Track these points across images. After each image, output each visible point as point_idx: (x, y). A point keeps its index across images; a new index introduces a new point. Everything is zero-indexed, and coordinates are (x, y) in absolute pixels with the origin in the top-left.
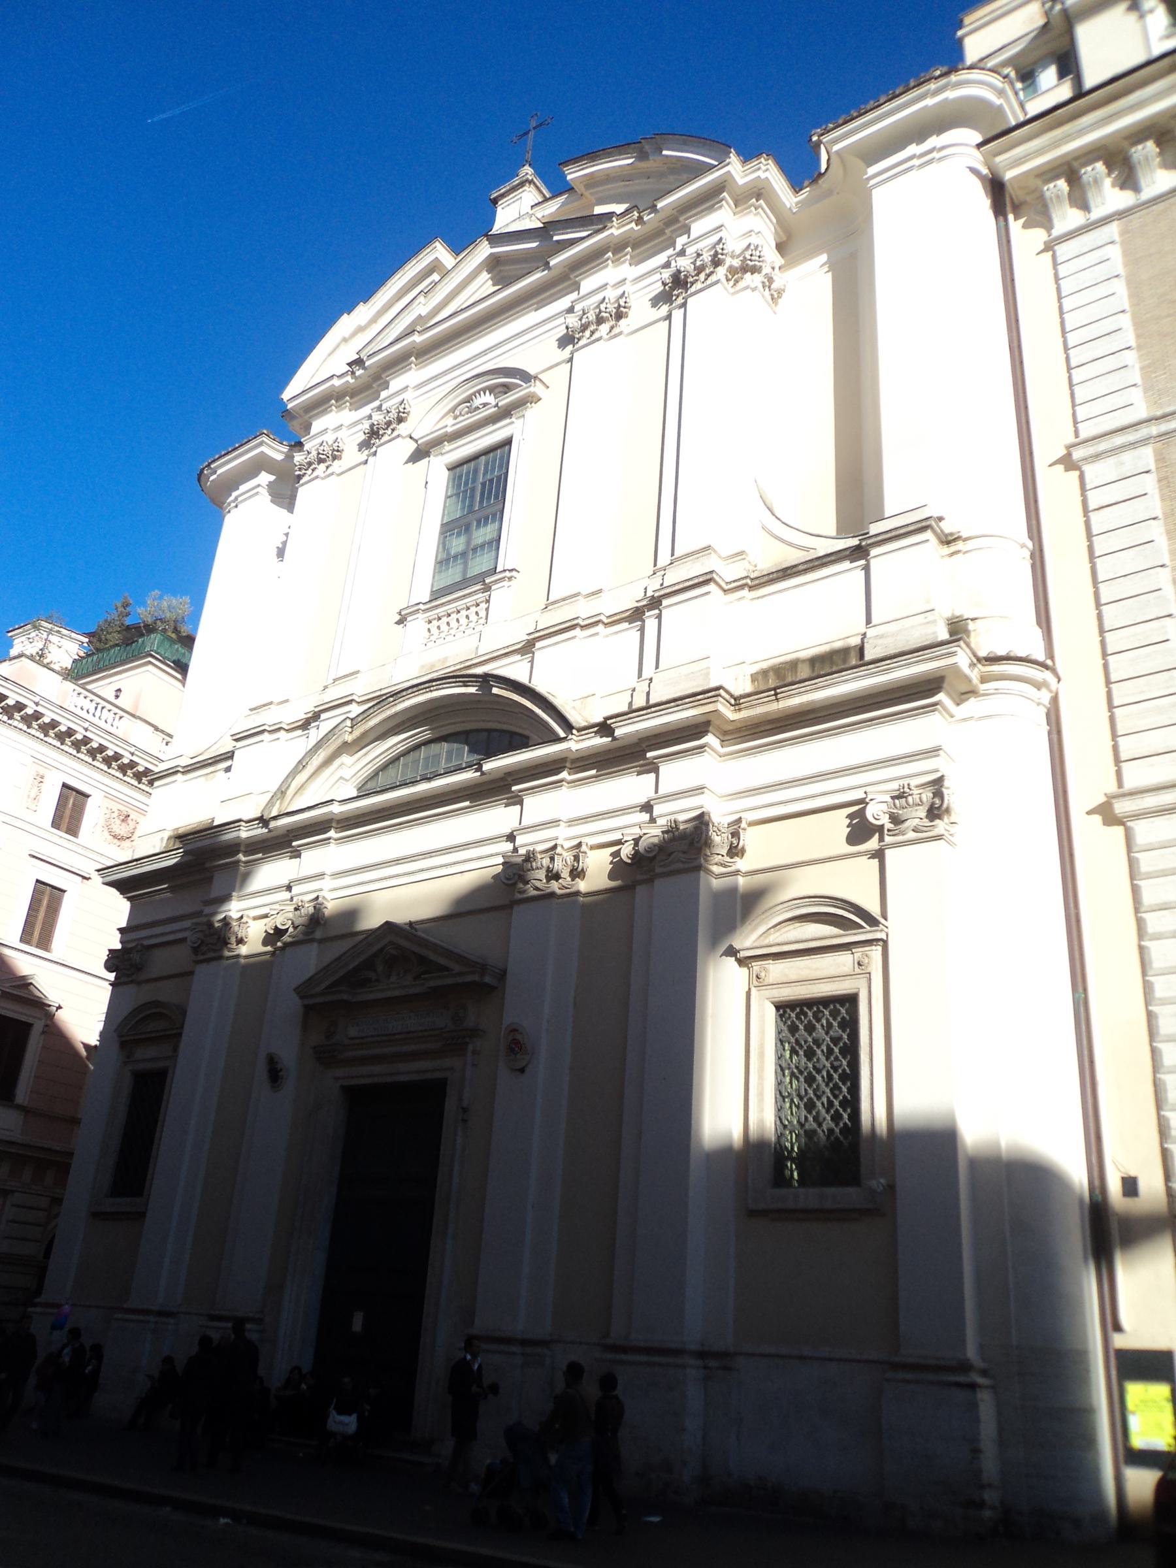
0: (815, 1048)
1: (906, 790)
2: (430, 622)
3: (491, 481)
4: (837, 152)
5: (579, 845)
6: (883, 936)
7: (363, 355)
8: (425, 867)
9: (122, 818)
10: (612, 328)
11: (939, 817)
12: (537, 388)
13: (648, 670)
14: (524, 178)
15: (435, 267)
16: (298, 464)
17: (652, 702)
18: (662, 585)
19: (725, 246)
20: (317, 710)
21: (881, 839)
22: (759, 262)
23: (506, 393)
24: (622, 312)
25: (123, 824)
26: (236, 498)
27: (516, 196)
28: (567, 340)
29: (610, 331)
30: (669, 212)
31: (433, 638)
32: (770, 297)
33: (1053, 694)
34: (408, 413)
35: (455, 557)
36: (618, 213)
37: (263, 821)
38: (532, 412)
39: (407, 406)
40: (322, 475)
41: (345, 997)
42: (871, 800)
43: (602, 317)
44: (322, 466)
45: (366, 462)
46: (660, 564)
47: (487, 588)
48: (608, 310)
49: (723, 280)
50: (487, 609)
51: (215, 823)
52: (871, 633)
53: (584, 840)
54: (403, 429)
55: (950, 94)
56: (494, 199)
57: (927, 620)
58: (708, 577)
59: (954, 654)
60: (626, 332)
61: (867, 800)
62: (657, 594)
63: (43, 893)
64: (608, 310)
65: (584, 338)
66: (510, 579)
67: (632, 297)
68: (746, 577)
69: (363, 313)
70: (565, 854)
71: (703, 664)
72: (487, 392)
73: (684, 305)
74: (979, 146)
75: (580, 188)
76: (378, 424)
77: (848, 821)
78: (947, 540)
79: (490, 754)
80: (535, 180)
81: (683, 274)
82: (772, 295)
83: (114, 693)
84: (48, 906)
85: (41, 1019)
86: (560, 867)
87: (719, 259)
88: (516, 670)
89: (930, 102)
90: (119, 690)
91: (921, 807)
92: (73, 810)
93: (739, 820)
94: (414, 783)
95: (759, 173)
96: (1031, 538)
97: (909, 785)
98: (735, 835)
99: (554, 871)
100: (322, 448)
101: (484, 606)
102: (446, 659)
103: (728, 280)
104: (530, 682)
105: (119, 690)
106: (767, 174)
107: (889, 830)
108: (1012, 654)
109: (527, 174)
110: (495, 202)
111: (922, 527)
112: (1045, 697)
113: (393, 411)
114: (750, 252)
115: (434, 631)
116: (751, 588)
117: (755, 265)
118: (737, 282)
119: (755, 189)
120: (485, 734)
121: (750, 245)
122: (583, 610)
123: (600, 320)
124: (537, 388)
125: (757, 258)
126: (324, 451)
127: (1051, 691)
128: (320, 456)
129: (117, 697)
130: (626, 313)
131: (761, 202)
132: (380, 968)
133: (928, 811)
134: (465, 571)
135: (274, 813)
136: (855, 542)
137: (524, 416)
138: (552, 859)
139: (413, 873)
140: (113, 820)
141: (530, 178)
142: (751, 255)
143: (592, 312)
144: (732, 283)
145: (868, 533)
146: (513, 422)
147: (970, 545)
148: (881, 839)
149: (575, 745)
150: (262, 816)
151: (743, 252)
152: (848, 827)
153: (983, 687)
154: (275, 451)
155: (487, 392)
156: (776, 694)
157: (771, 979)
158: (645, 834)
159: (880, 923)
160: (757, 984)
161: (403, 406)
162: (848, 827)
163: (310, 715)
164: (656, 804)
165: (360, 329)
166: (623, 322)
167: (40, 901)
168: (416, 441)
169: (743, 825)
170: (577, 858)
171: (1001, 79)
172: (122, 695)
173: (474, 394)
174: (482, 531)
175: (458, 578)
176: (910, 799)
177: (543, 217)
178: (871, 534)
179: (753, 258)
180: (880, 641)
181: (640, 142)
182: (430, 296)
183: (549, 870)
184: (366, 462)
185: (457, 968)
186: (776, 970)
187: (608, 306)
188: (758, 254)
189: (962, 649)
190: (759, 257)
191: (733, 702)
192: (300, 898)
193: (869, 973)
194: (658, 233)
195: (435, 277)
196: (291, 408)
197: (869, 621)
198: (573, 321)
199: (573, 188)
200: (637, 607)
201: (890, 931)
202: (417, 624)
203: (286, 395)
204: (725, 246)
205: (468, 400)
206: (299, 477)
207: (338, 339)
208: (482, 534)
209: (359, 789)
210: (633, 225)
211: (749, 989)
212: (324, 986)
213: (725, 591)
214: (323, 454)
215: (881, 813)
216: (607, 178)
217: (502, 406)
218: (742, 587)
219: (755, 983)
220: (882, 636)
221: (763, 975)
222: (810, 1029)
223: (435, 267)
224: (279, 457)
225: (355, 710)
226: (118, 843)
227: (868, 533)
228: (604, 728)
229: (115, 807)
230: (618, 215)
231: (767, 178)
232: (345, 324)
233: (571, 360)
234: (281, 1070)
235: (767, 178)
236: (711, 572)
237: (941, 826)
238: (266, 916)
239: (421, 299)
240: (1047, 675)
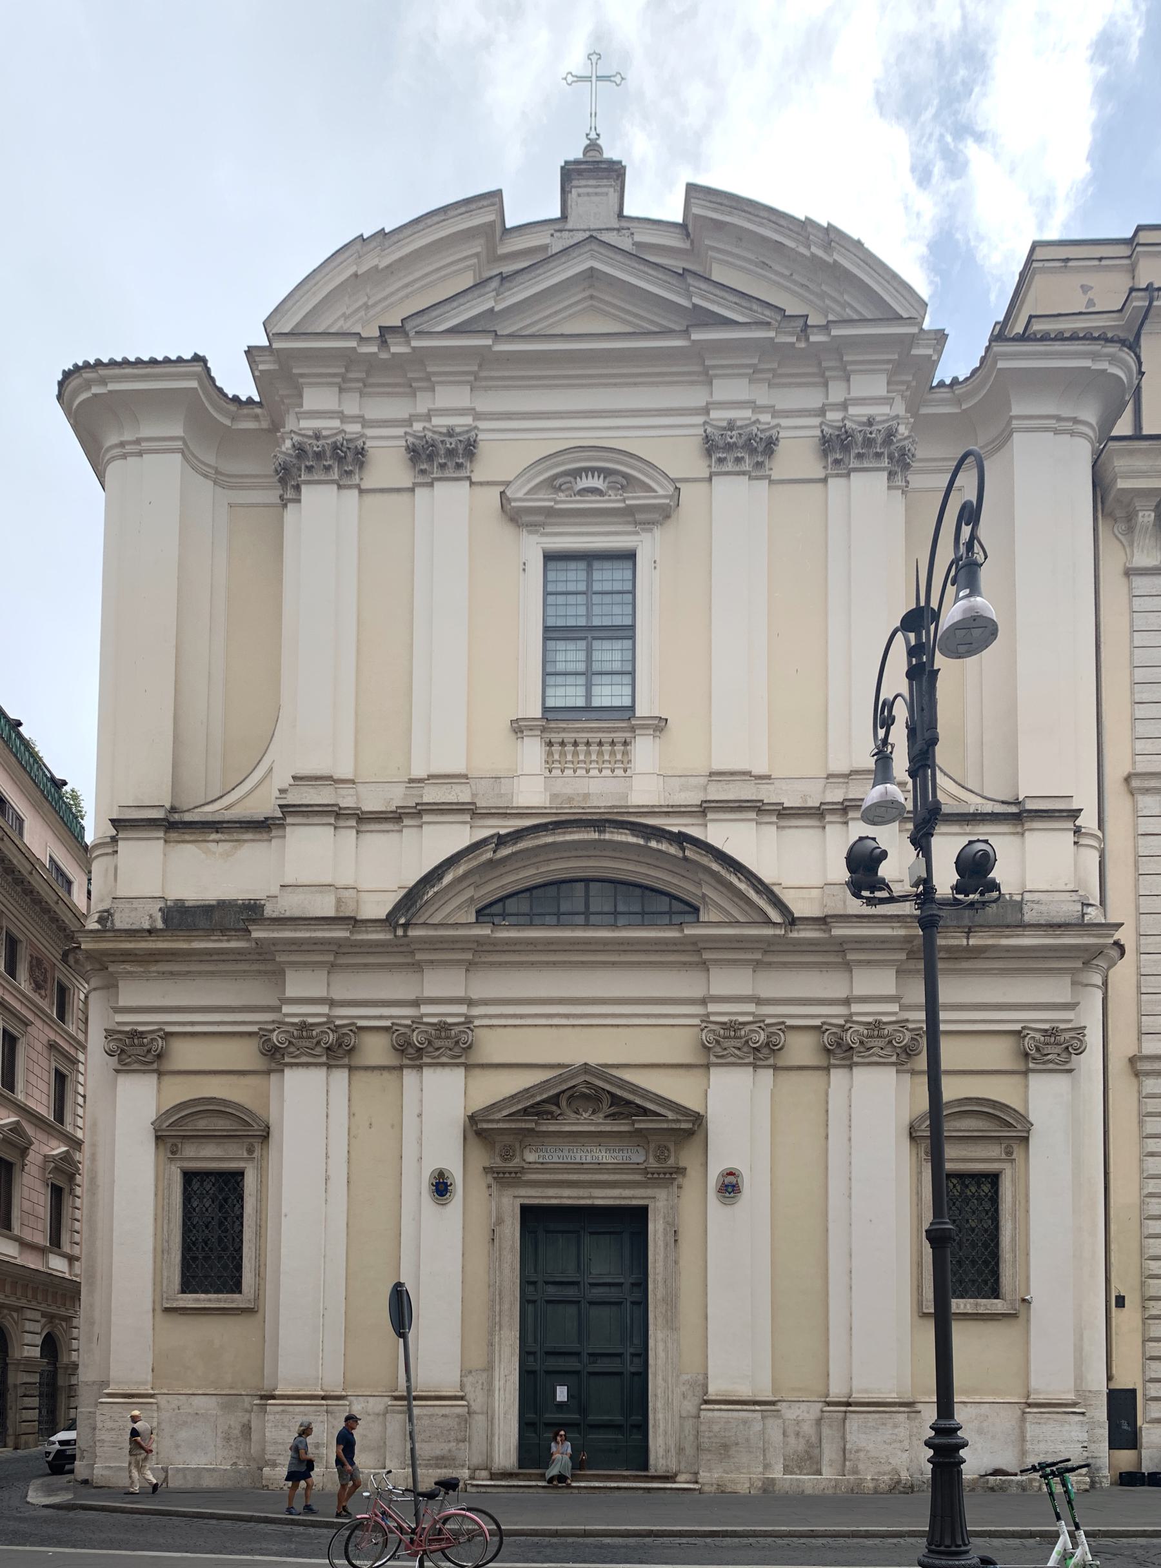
26: (138, 441)
41: (533, 1125)
57: (1073, 899)
72: (590, 474)
132: (564, 1103)
134: (588, 696)
155: (590, 474)
180: (1035, 906)
185: (671, 1115)
186: (189, 1150)
212: (505, 1113)
234: (451, 1184)
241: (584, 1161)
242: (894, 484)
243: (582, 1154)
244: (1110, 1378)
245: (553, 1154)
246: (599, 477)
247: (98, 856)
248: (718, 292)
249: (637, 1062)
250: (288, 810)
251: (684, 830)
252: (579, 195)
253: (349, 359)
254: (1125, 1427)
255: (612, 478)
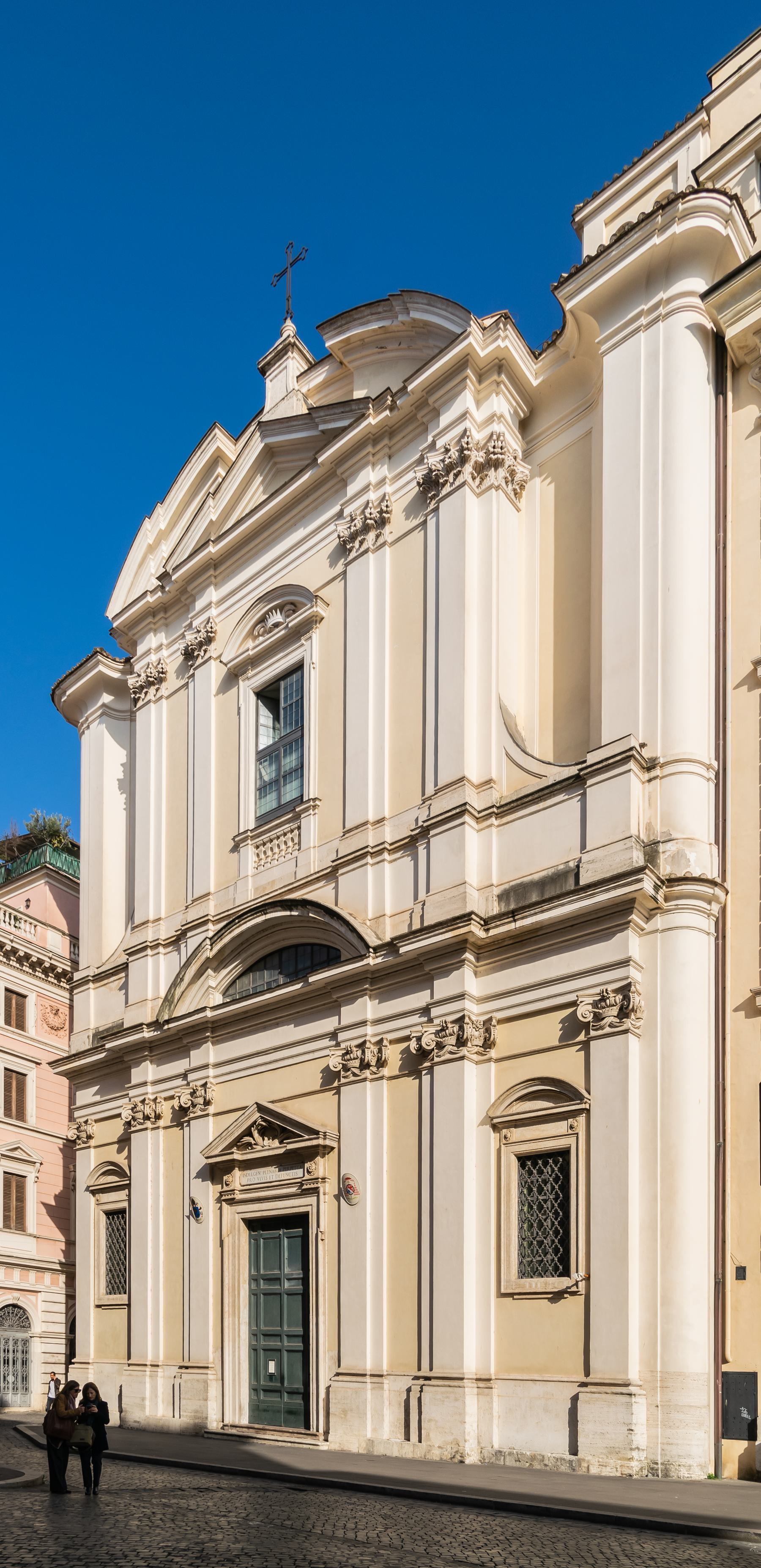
0: (543, 1186)
1: (605, 994)
2: (257, 847)
3: (291, 705)
4: (571, 311)
5: (382, 1040)
6: (587, 1107)
7: (169, 568)
8: (278, 1058)
9: (54, 1012)
10: (378, 536)
11: (627, 1016)
12: (319, 609)
13: (422, 895)
14: (287, 342)
15: (217, 458)
16: (131, 687)
17: (426, 924)
18: (429, 815)
19: (470, 440)
20: (183, 928)
21: (587, 1033)
22: (501, 454)
23: (294, 612)
24: (384, 518)
25: (56, 1017)
27: (281, 364)
28: (343, 549)
29: (376, 541)
30: (418, 395)
31: (262, 862)
32: (513, 493)
33: (722, 905)
34: (215, 632)
35: (270, 784)
36: (373, 398)
37: (156, 1024)
38: (316, 635)
39: (213, 625)
40: (153, 699)
42: (581, 1002)
43: (368, 524)
44: (152, 690)
45: (187, 684)
46: (428, 794)
47: (297, 817)
48: (372, 516)
49: (470, 480)
50: (300, 835)
51: (125, 1026)
52: (585, 858)
53: (384, 1036)
54: (213, 650)
55: (677, 229)
56: (263, 367)
58: (463, 808)
59: (640, 880)
60: (390, 540)
61: (578, 1002)
62: (425, 824)
63: (11, 1078)
64: (372, 516)
65: (355, 550)
66: (315, 807)
67: (393, 499)
68: (492, 807)
69: (162, 515)
70: (372, 1047)
71: (461, 889)
73: (436, 509)
74: (704, 296)
75: (338, 354)
76: (191, 645)
77: (561, 1025)
78: (650, 766)
79: (315, 968)
80: (297, 342)
81: (434, 473)
82: (514, 490)
83: (25, 904)
84: (17, 1088)
85: (31, 1172)
86: (370, 1058)
87: (465, 455)
88: (322, 894)
89: (656, 240)
90: (28, 900)
91: (615, 1007)
92: (17, 1009)
93: (490, 1019)
94: (262, 993)
95: (499, 342)
96: (717, 758)
97: (606, 990)
98: (488, 1031)
99: (366, 1061)
100: (149, 670)
101: (296, 832)
102: (273, 882)
103: (474, 478)
104: (336, 905)
105: (28, 900)
106: (507, 343)
107: (593, 1026)
108: (688, 875)
109: (289, 336)
110: (263, 372)
111: (626, 757)
112: (715, 908)
113: (203, 631)
114: (493, 444)
115: (262, 856)
116: (498, 816)
117: (497, 459)
118: (483, 480)
119: (497, 361)
120: (309, 948)
121: (492, 434)
122: (371, 838)
123: (366, 529)
124: (319, 609)
125: (499, 450)
126: (151, 673)
127: (720, 903)
128: (149, 679)
129: (28, 906)
130: (389, 518)
131: (503, 376)
132: (256, 1134)
133: (620, 1010)
134: (279, 798)
135: (166, 1017)
136: (573, 771)
137: (311, 637)
138: (363, 1052)
139: (270, 1063)
140: (48, 1015)
141: (292, 341)
142: (494, 447)
143: (359, 518)
144: (478, 480)
145: (585, 762)
146: (303, 645)
147: (668, 770)
148: (587, 1033)
149: (372, 961)
150: (157, 1020)
151: (486, 444)
152: (560, 1030)
153: (665, 905)
154: (109, 668)
156: (513, 916)
157: (513, 1139)
158: (426, 1032)
159: (584, 1097)
160: (505, 1142)
161: (210, 625)
162: (560, 1030)
163: (179, 932)
164: (468, 965)
165: (162, 536)
166: (387, 529)
167: (11, 1084)
168: (226, 665)
169: (494, 1022)
170: (380, 1051)
171: (728, 201)
172: (32, 904)
173: (267, 613)
174: (288, 760)
175: (274, 805)
176: (608, 1001)
177: (309, 390)
178: (588, 763)
179: (496, 450)
181: (388, 300)
182: (218, 496)
183: (362, 1060)
184: (187, 684)
186: (517, 1134)
187: (373, 510)
188: (500, 444)
189: (647, 875)
190: (502, 448)
191: (482, 922)
192: (194, 1083)
193: (577, 1134)
194: (410, 419)
195: (221, 471)
196: (117, 627)
197: (583, 846)
198: (343, 528)
199: (331, 355)
200: (411, 836)
201: (592, 1102)
202: (249, 851)
203: (112, 611)
204: (470, 440)
205: (263, 620)
206: (136, 701)
207: (144, 548)
208: (289, 762)
209: (225, 993)
210: (387, 412)
211: (500, 1146)
212: (220, 1149)
213: (477, 819)
214: (151, 677)
215: (587, 1013)
216: (363, 343)
217: (292, 627)
218: (489, 816)
219: (504, 1142)
220: (593, 861)
221: (509, 1135)
222: (540, 1172)
223: (217, 458)
224: (116, 675)
225: (212, 929)
226: (55, 1033)
227: (585, 762)
228: (391, 946)
229: (47, 1003)
230: (373, 400)
231: (506, 347)
232: (149, 530)
233: (344, 573)
235: (506, 347)
236: (465, 804)
237: (628, 1023)
238: (172, 1098)
239: (210, 502)
240: (718, 891)
241: (271, 1180)
242: (529, 438)
243: (271, 1174)
244: (720, 1357)
245: (256, 1177)
246: (276, 613)
247: (342, 874)
248: (332, 412)
249: (286, 1096)
250: (132, 952)
251: (305, 897)
252: (271, 381)
253: (152, 612)
254: (745, 1414)
255: (286, 608)
